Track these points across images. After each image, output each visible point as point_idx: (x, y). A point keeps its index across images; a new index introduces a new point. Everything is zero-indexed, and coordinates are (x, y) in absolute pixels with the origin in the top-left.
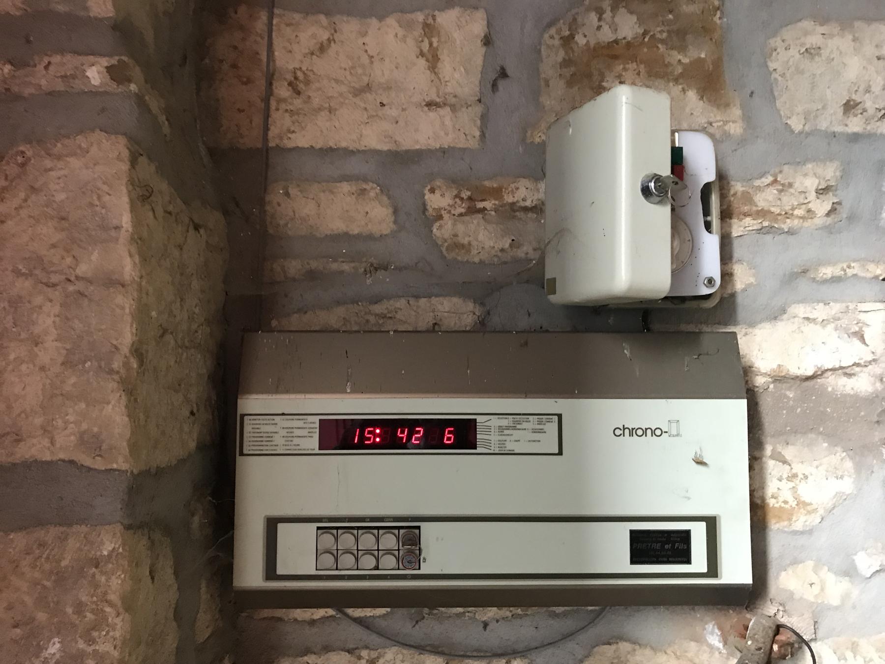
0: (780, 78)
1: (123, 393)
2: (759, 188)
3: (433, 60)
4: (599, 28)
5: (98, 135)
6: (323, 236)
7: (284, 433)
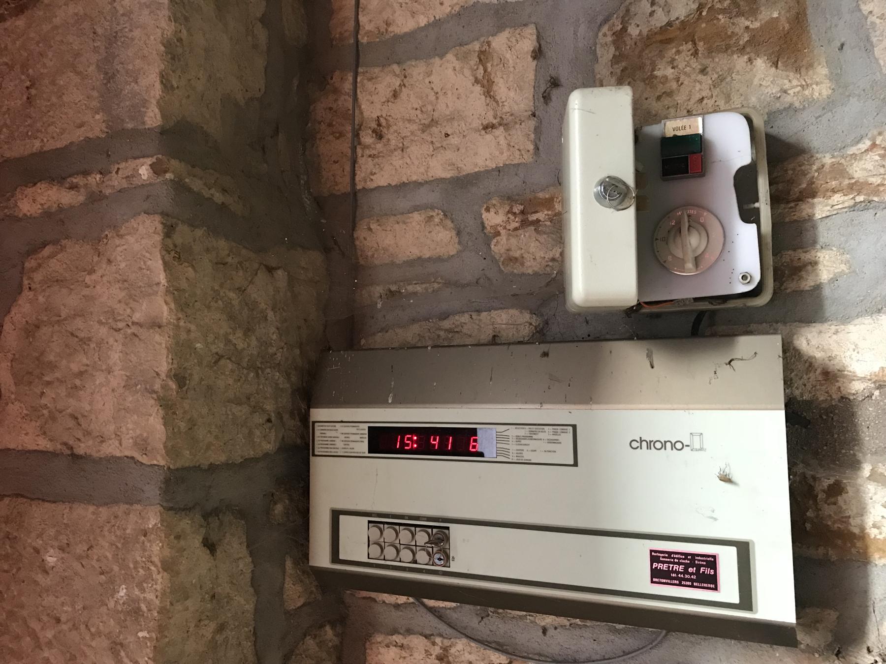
0: (878, 21)
1: (160, 408)
2: (854, 156)
3: (487, 86)
4: (652, 14)
5: (143, 217)
6: (401, 262)
7: (342, 437)
